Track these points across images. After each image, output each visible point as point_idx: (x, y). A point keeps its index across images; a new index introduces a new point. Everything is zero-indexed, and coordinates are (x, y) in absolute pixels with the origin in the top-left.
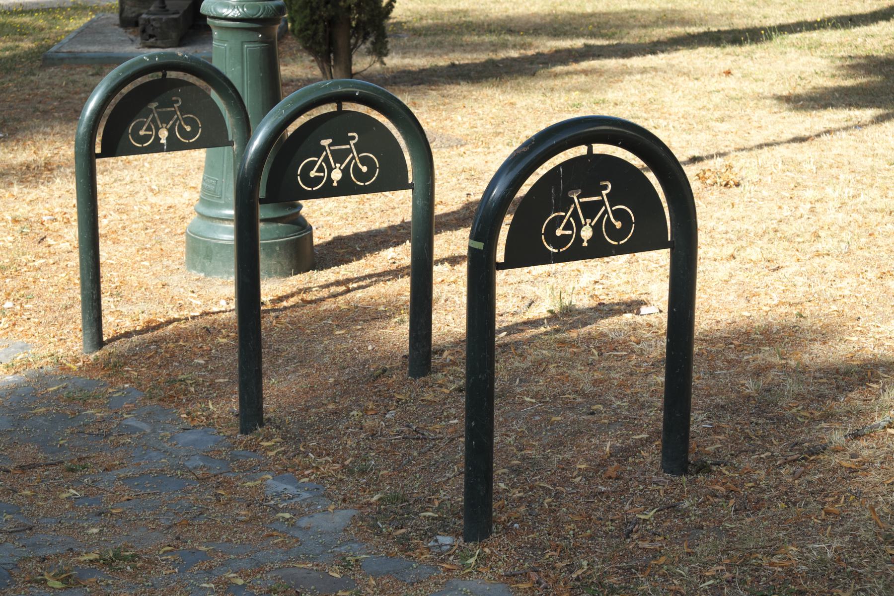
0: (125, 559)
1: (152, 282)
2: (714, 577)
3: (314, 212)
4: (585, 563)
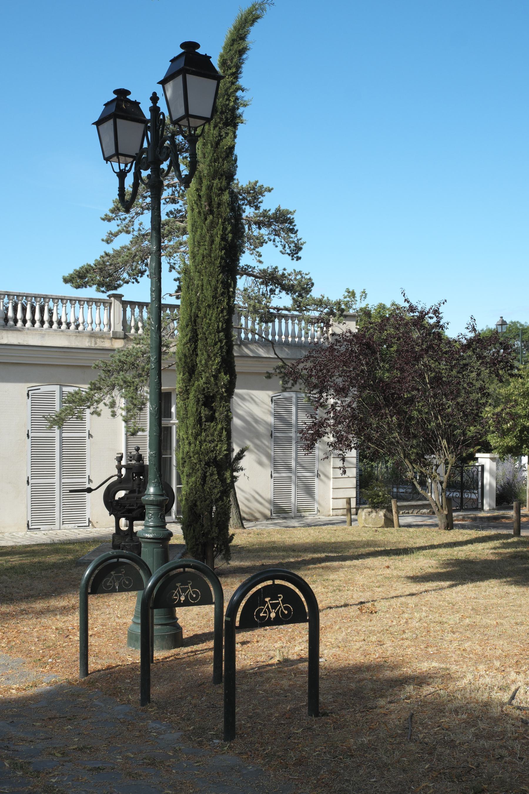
0: (87, 748)
1: (112, 651)
2: (319, 751)
3: (187, 625)
4: (270, 748)
